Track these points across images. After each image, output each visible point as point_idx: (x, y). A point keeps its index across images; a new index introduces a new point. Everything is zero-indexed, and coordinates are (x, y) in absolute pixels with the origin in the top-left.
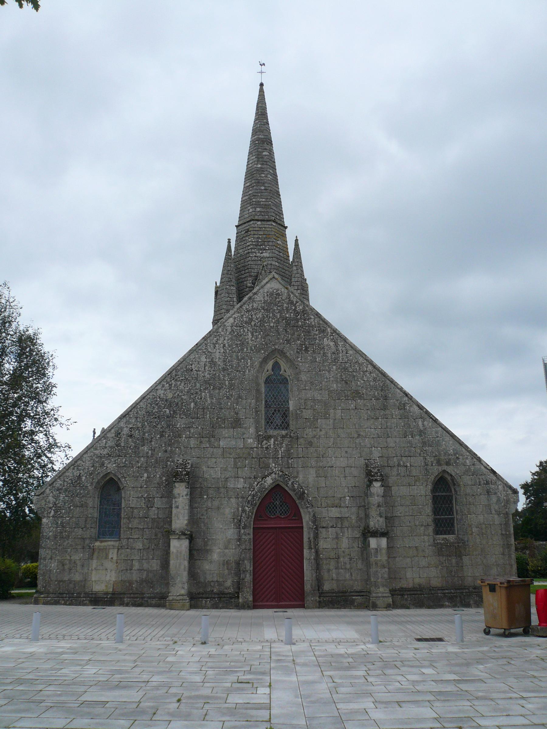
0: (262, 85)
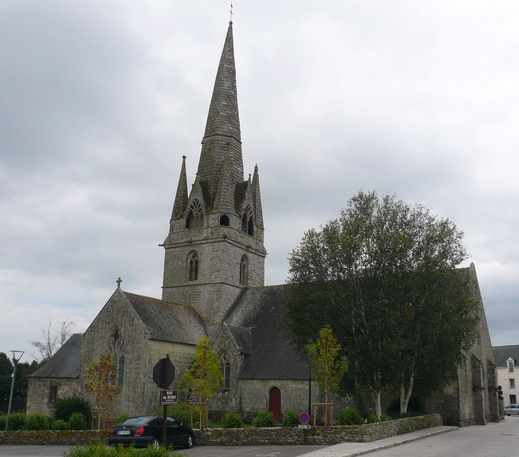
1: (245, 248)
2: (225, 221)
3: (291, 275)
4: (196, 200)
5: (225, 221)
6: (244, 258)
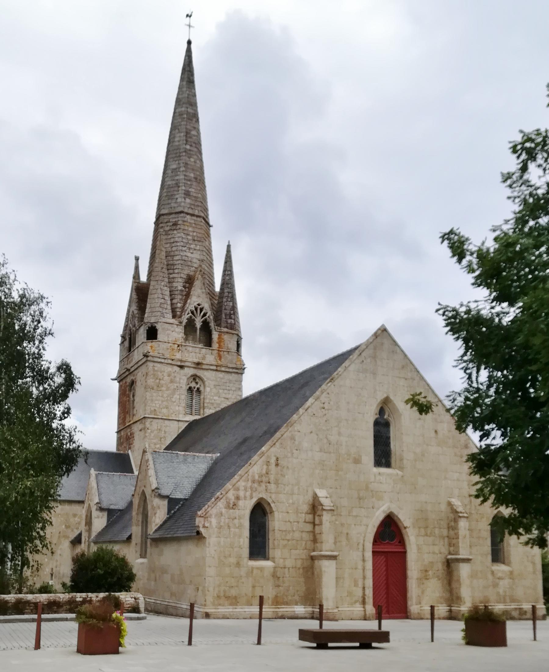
0: (189, 43)
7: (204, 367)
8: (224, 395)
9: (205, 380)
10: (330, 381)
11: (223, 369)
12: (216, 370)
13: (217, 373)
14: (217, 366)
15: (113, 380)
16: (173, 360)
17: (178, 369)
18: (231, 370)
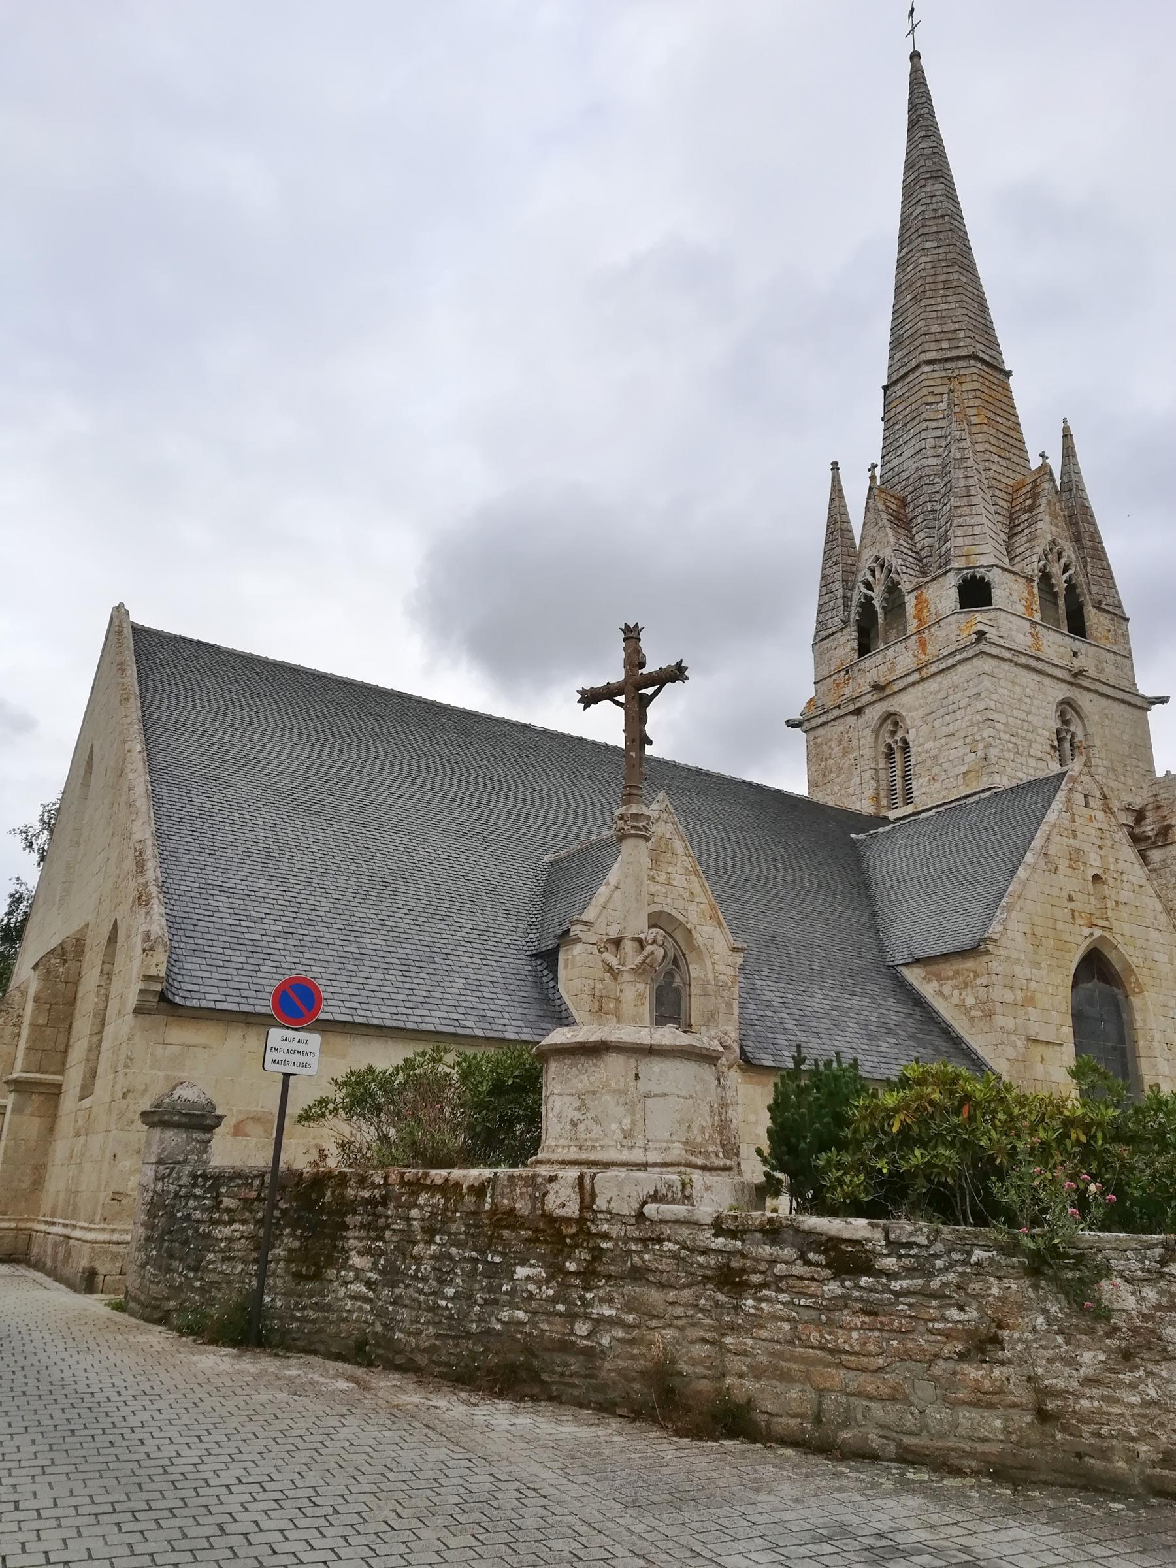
1: (1067, 677)
2: (975, 593)
3: (1148, 1081)
4: (877, 558)
5: (975, 593)
6: (1067, 708)
7: (896, 687)
8: (945, 730)
9: (904, 714)
10: (852, 713)
11: (933, 669)
12: (922, 680)
13: (926, 685)
14: (919, 670)
15: (1163, 700)
16: (839, 707)
17: (851, 720)
18: (950, 662)
